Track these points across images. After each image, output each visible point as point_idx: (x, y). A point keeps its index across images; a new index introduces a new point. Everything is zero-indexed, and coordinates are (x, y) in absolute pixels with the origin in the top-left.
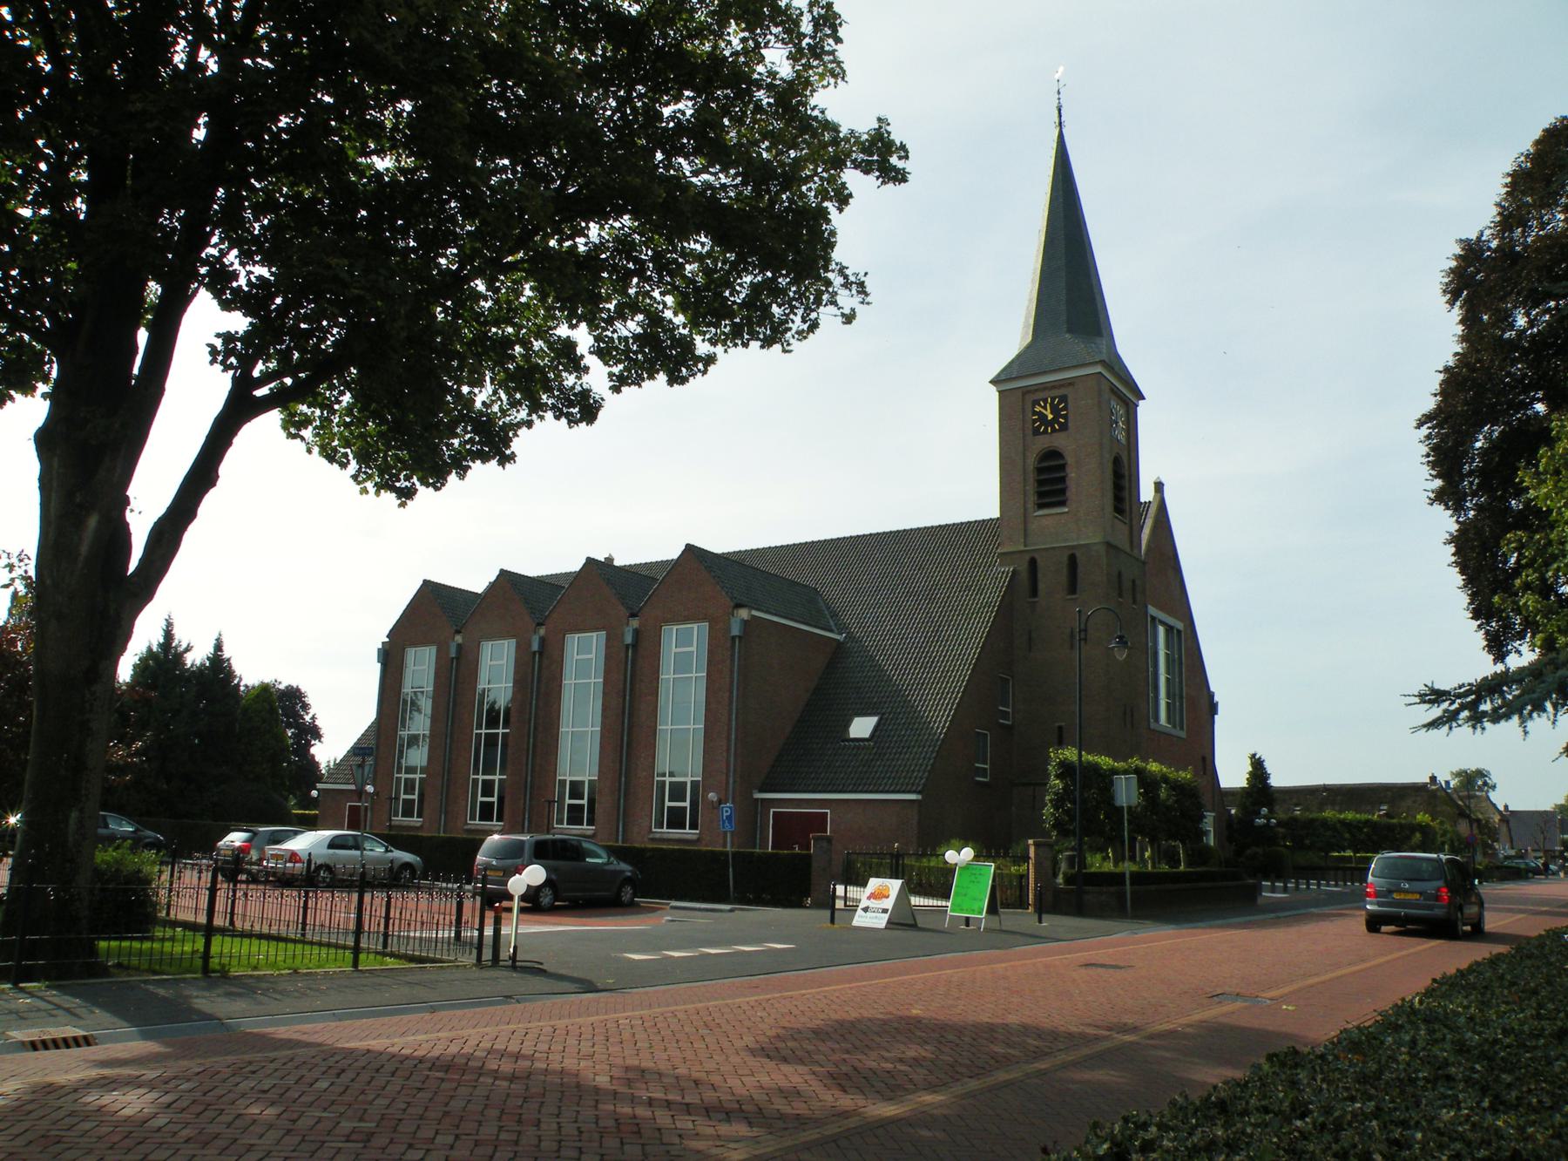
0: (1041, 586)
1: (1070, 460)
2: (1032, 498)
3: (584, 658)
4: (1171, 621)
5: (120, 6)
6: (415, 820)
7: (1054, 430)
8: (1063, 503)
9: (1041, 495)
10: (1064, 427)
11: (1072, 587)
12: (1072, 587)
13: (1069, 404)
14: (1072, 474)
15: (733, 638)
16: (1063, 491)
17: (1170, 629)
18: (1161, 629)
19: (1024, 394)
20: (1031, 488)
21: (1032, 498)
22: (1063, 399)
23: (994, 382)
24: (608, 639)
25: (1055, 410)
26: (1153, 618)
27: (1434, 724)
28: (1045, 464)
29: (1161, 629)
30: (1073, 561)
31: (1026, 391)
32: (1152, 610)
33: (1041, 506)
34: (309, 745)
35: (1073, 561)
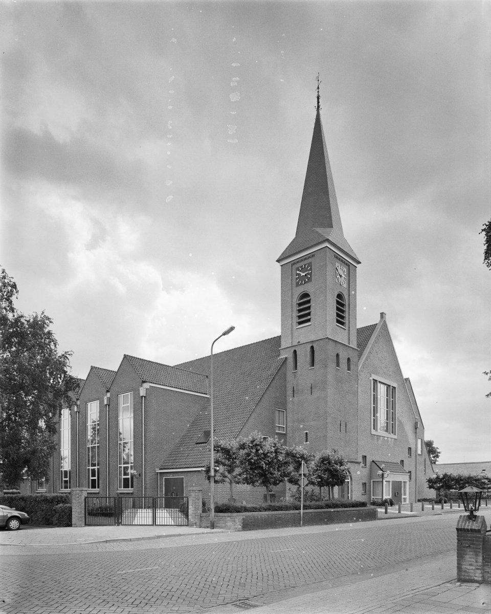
2: (296, 320)
6: (130, 490)
8: (309, 320)
15: (142, 397)
18: (382, 389)
19: (292, 265)
22: (310, 264)
23: (278, 261)
26: (375, 381)
29: (382, 389)
31: (293, 263)
33: (300, 323)
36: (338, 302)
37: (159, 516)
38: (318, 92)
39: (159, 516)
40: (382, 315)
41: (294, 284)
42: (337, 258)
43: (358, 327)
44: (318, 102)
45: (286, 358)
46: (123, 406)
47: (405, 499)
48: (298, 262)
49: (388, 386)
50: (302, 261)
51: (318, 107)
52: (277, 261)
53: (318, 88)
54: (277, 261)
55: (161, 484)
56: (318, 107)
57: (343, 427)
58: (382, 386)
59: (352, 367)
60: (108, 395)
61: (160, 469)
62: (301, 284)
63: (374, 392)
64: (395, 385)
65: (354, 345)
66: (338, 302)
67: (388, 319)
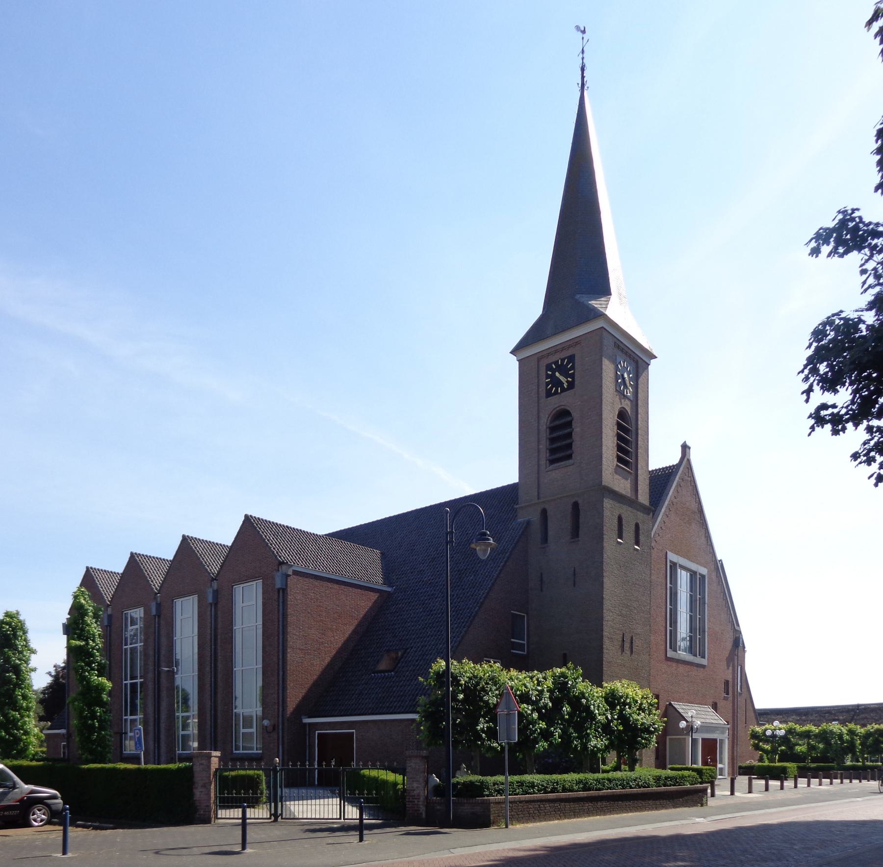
0: (551, 533)
1: (575, 415)
2: (545, 455)
3: (186, 617)
4: (694, 567)
8: (569, 457)
9: (552, 451)
11: (575, 532)
13: (576, 369)
14: (577, 429)
15: (279, 590)
16: (569, 446)
17: (693, 574)
18: (683, 578)
19: (539, 360)
20: (544, 445)
22: (571, 359)
23: (513, 352)
24: (199, 601)
26: (674, 565)
28: (557, 423)
29: (683, 578)
30: (576, 506)
32: (672, 557)
33: (552, 462)
34: (64, 668)
35: (576, 506)
36: (618, 424)
37: (335, 806)
38: (583, 58)
39: (335, 806)
40: (685, 448)
41: (543, 393)
42: (618, 347)
43: (650, 469)
44: (583, 77)
45: (528, 523)
46: (242, 605)
47: (721, 769)
49: (693, 574)
50: (556, 352)
51: (583, 85)
52: (656, 357)
53: (583, 52)
54: (656, 357)
55: (312, 746)
56: (583, 85)
57: (627, 645)
58: (684, 573)
59: (642, 538)
60: (215, 585)
61: (309, 717)
62: (556, 393)
63: (671, 583)
64: (703, 571)
65: (644, 498)
66: (619, 426)
67: (695, 458)
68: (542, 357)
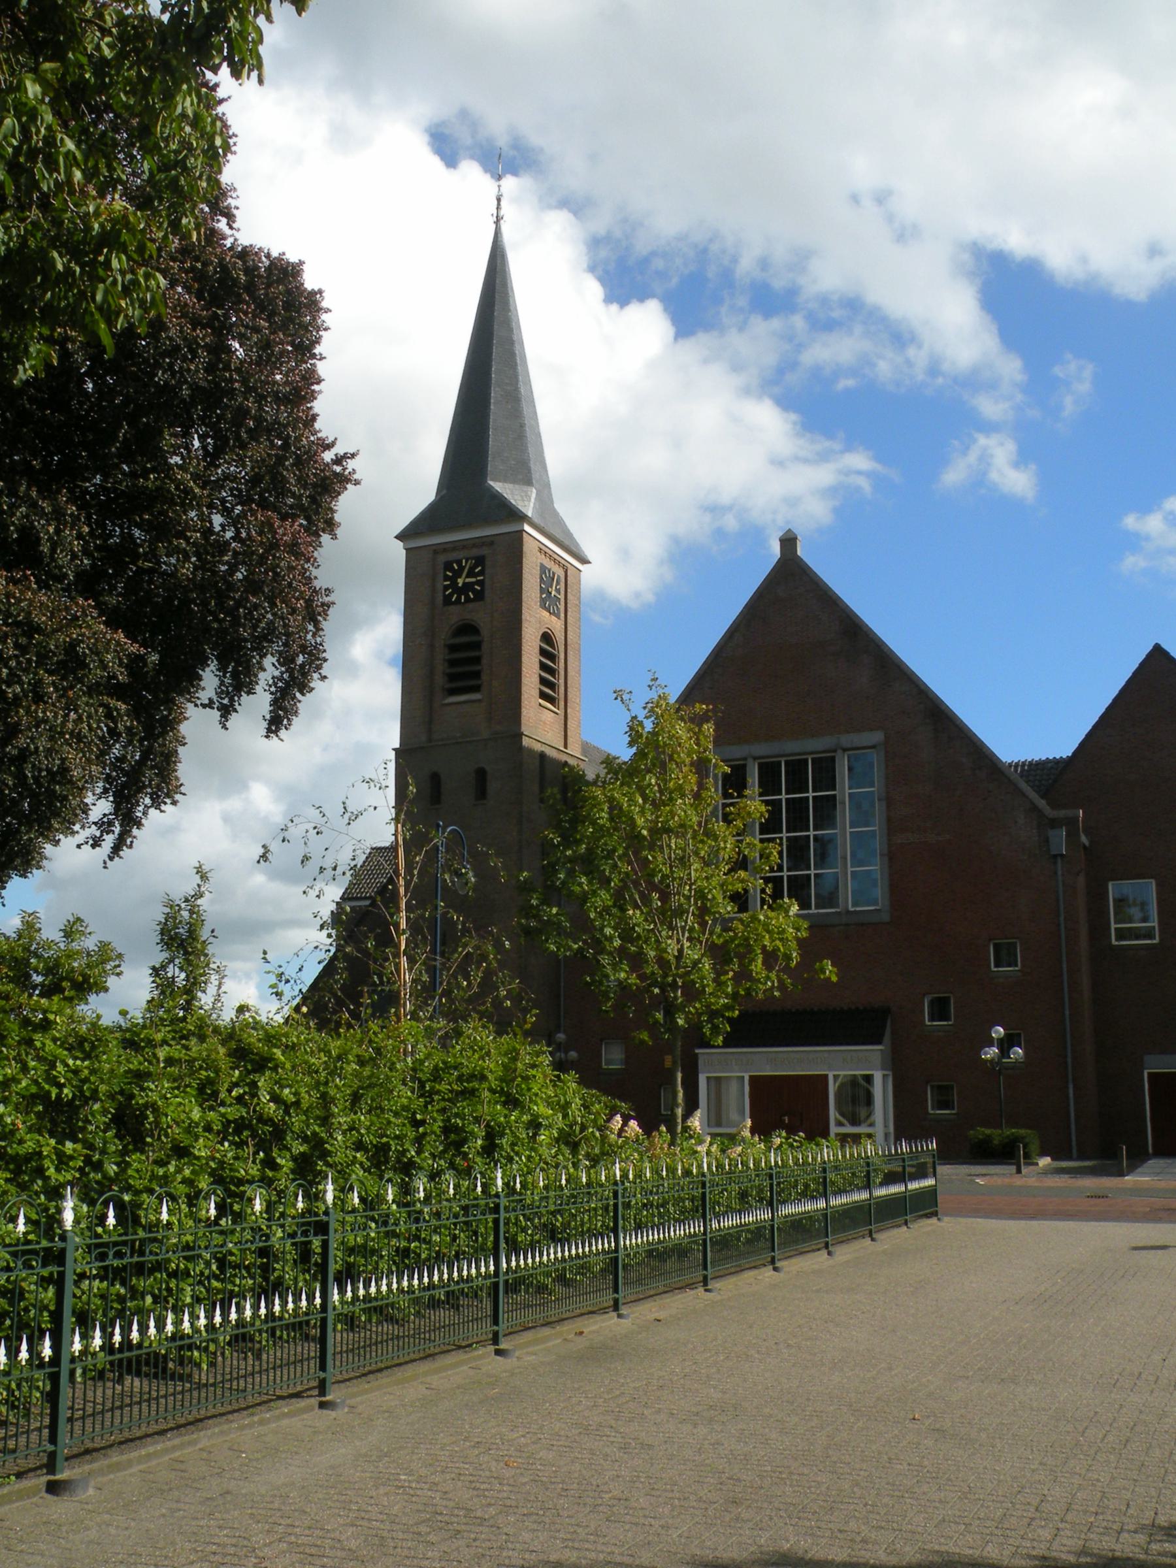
1: (485, 632)
5: (165, 7)
7: (468, 600)
8: (476, 689)
9: (452, 677)
10: (480, 596)
12: (481, 775)
16: (477, 675)
19: (436, 552)
21: (440, 680)
22: (480, 560)
25: (467, 587)
27: (116, 849)
28: (458, 640)
31: (437, 550)
33: (453, 692)
44: (498, 208)
48: (454, 549)
68: (445, 550)
